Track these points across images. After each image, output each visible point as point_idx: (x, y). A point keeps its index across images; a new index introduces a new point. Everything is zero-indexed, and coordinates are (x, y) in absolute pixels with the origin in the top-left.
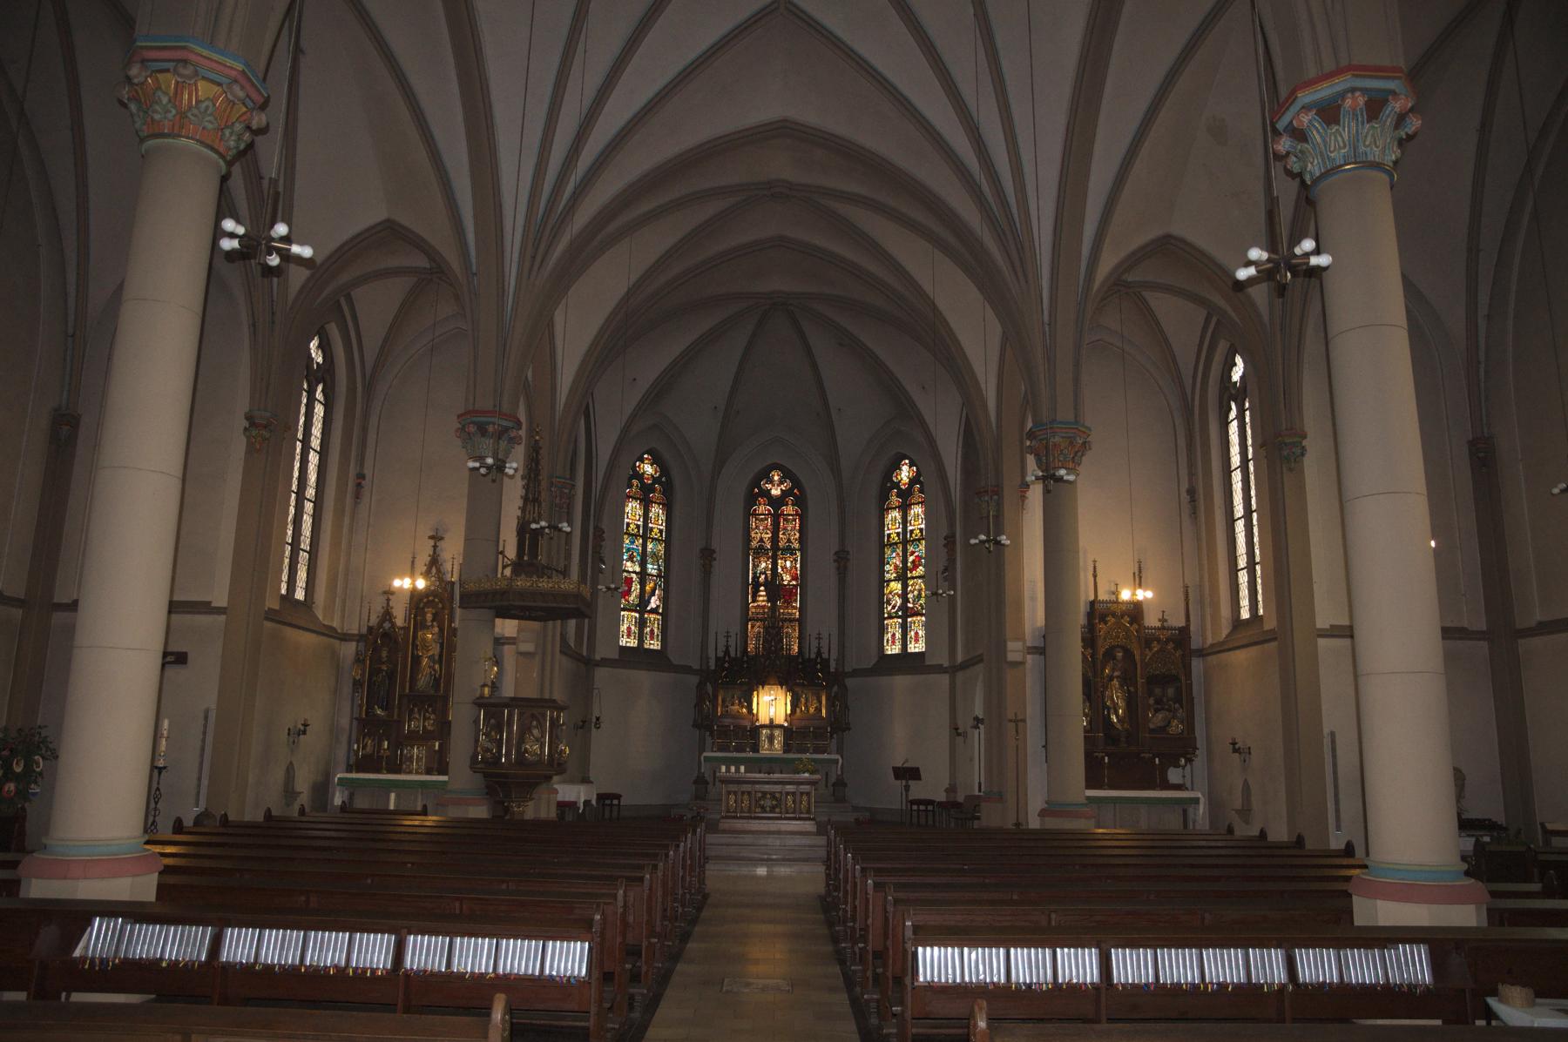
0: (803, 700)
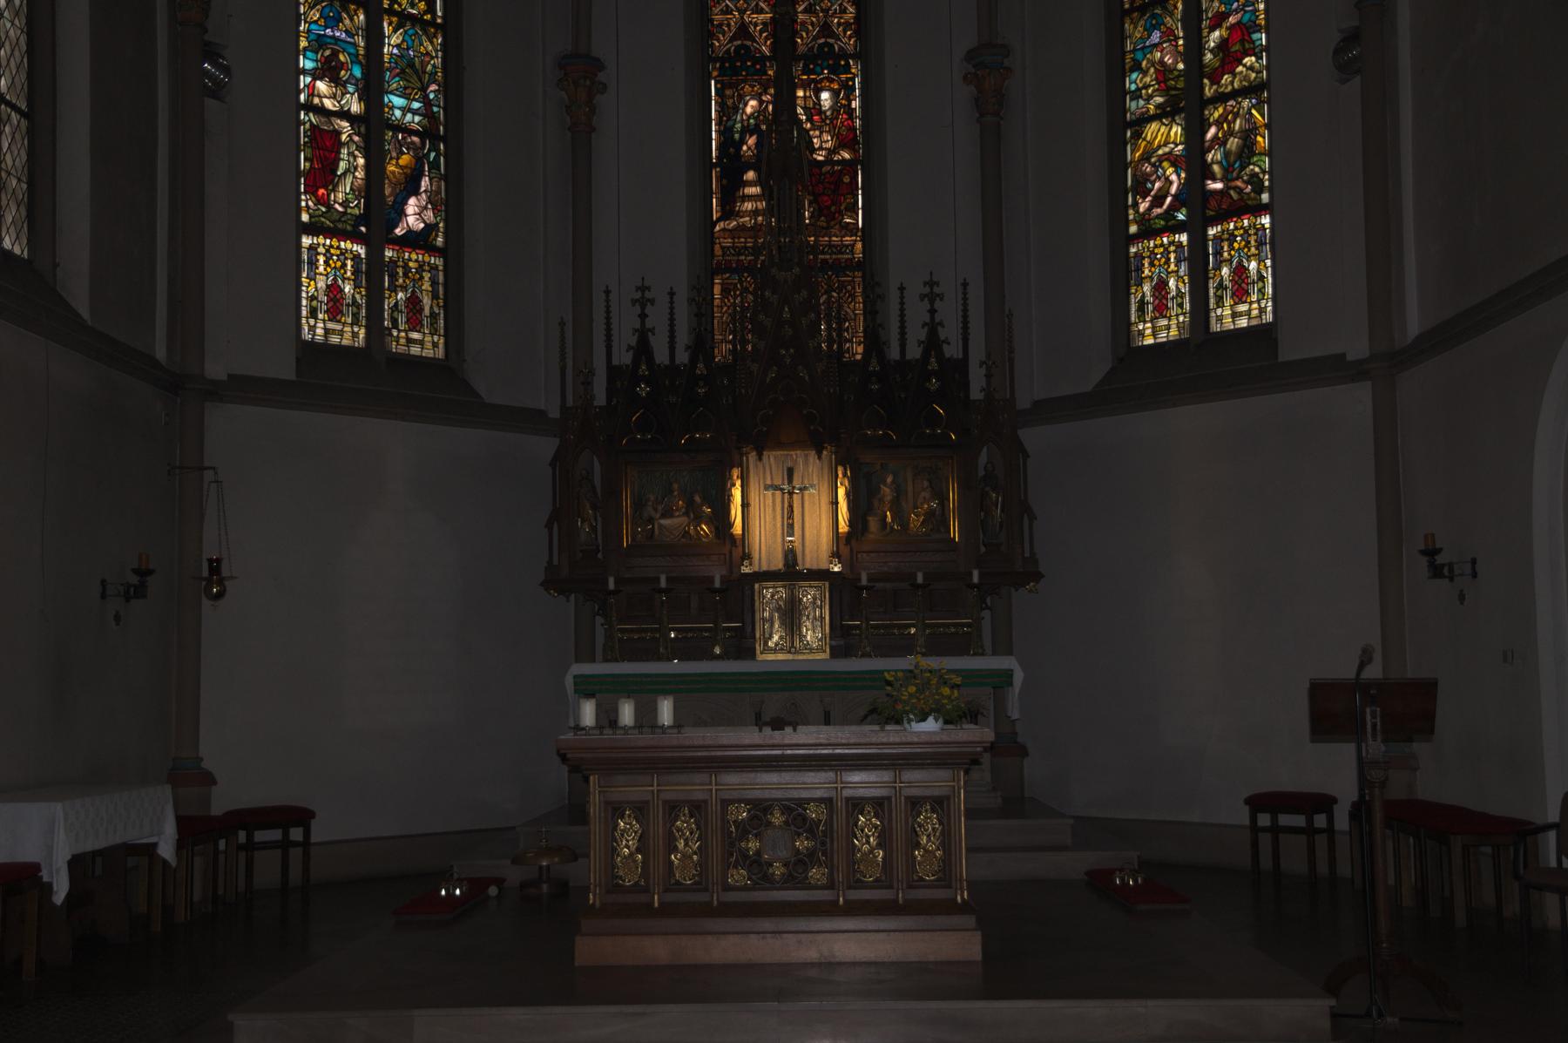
0: (887, 492)
